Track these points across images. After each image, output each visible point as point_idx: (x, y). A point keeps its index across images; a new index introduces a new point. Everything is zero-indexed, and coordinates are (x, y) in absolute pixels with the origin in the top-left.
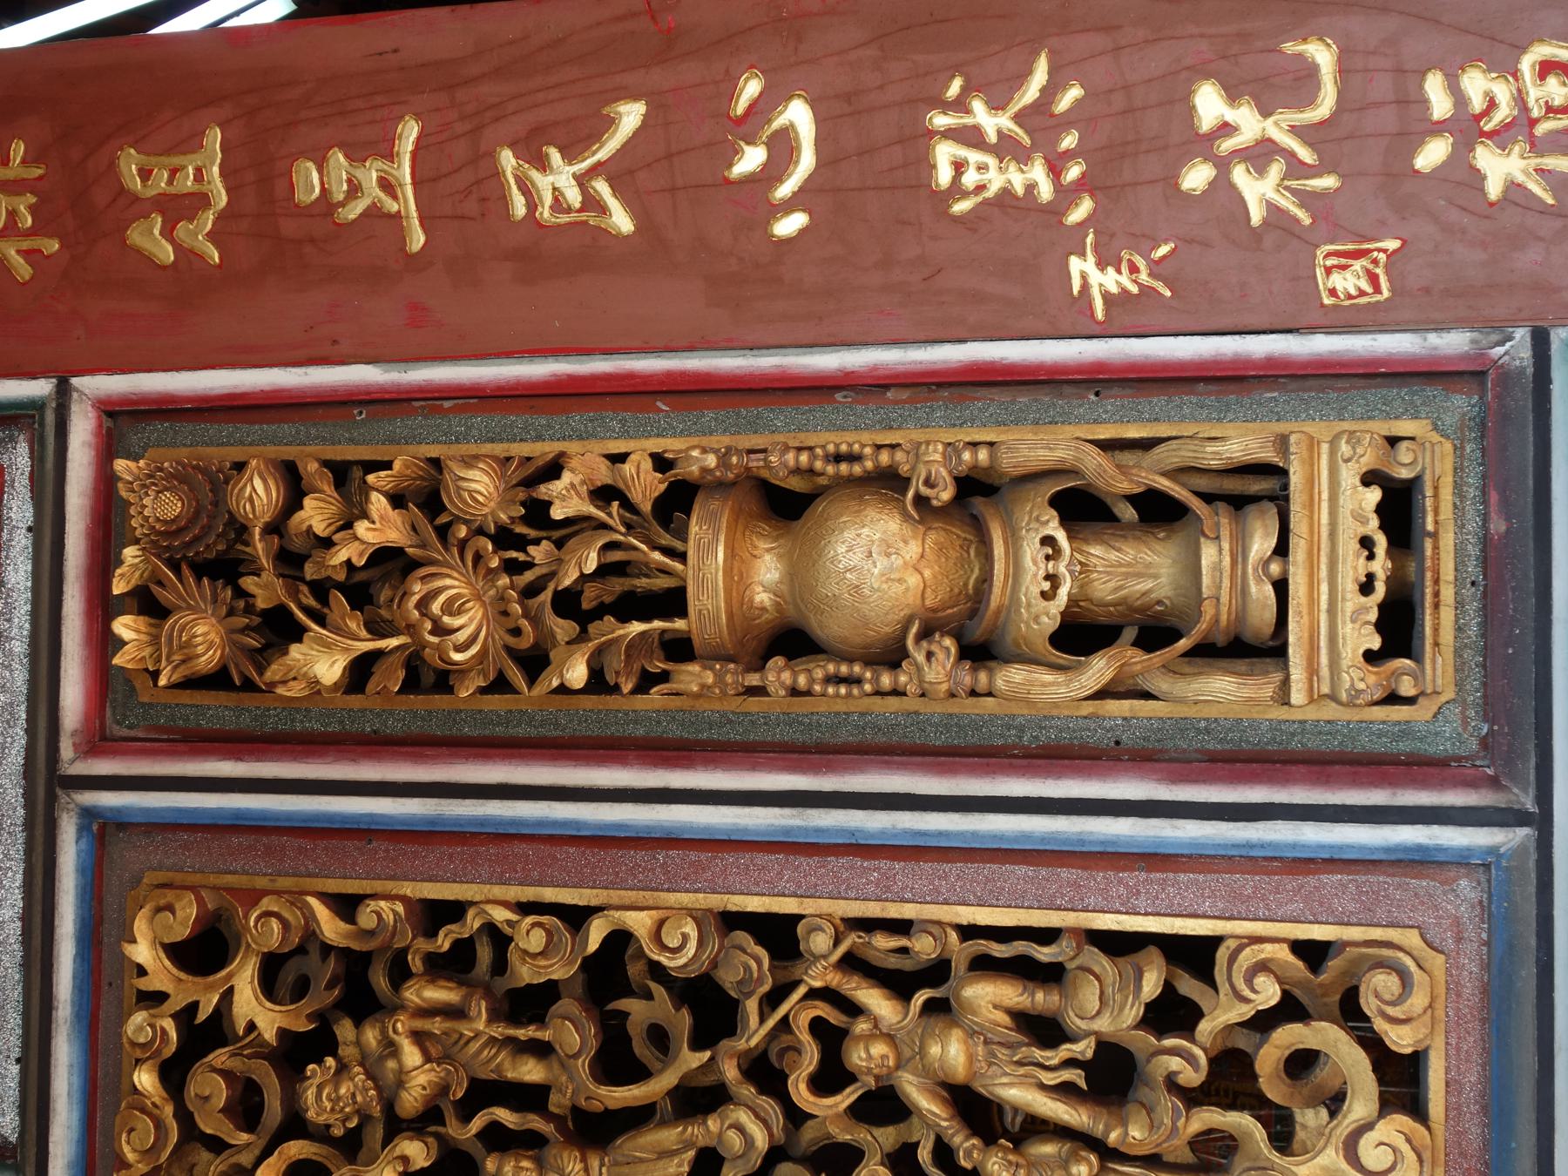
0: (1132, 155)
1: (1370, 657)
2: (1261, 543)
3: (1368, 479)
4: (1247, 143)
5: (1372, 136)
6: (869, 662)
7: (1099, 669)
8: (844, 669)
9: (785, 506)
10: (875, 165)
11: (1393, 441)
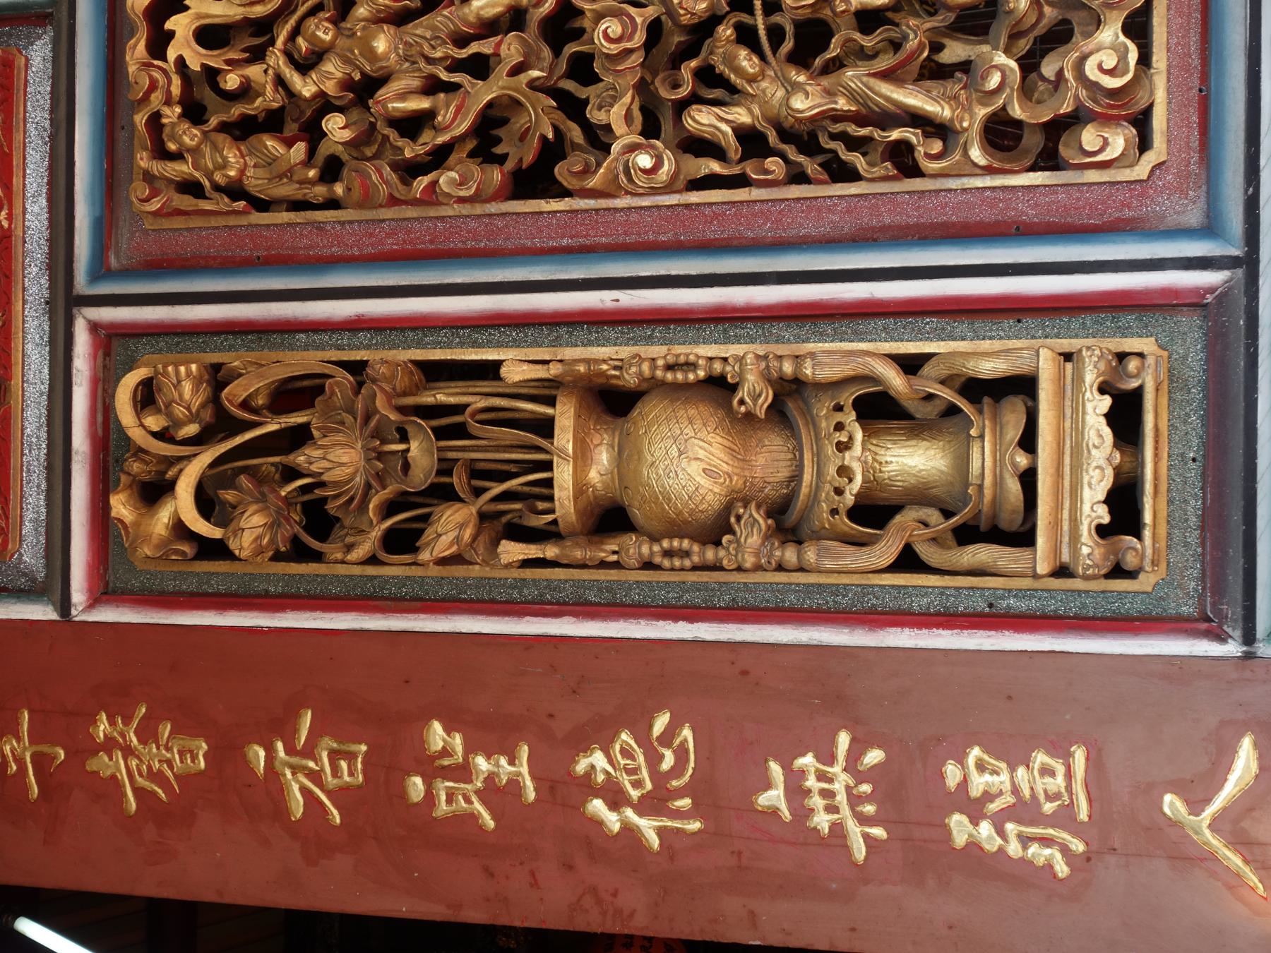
1: (1102, 531)
2: (1014, 431)
3: (1102, 390)
6: (693, 539)
7: (886, 550)
8: (680, 376)
9: (613, 402)
11: (1122, 357)
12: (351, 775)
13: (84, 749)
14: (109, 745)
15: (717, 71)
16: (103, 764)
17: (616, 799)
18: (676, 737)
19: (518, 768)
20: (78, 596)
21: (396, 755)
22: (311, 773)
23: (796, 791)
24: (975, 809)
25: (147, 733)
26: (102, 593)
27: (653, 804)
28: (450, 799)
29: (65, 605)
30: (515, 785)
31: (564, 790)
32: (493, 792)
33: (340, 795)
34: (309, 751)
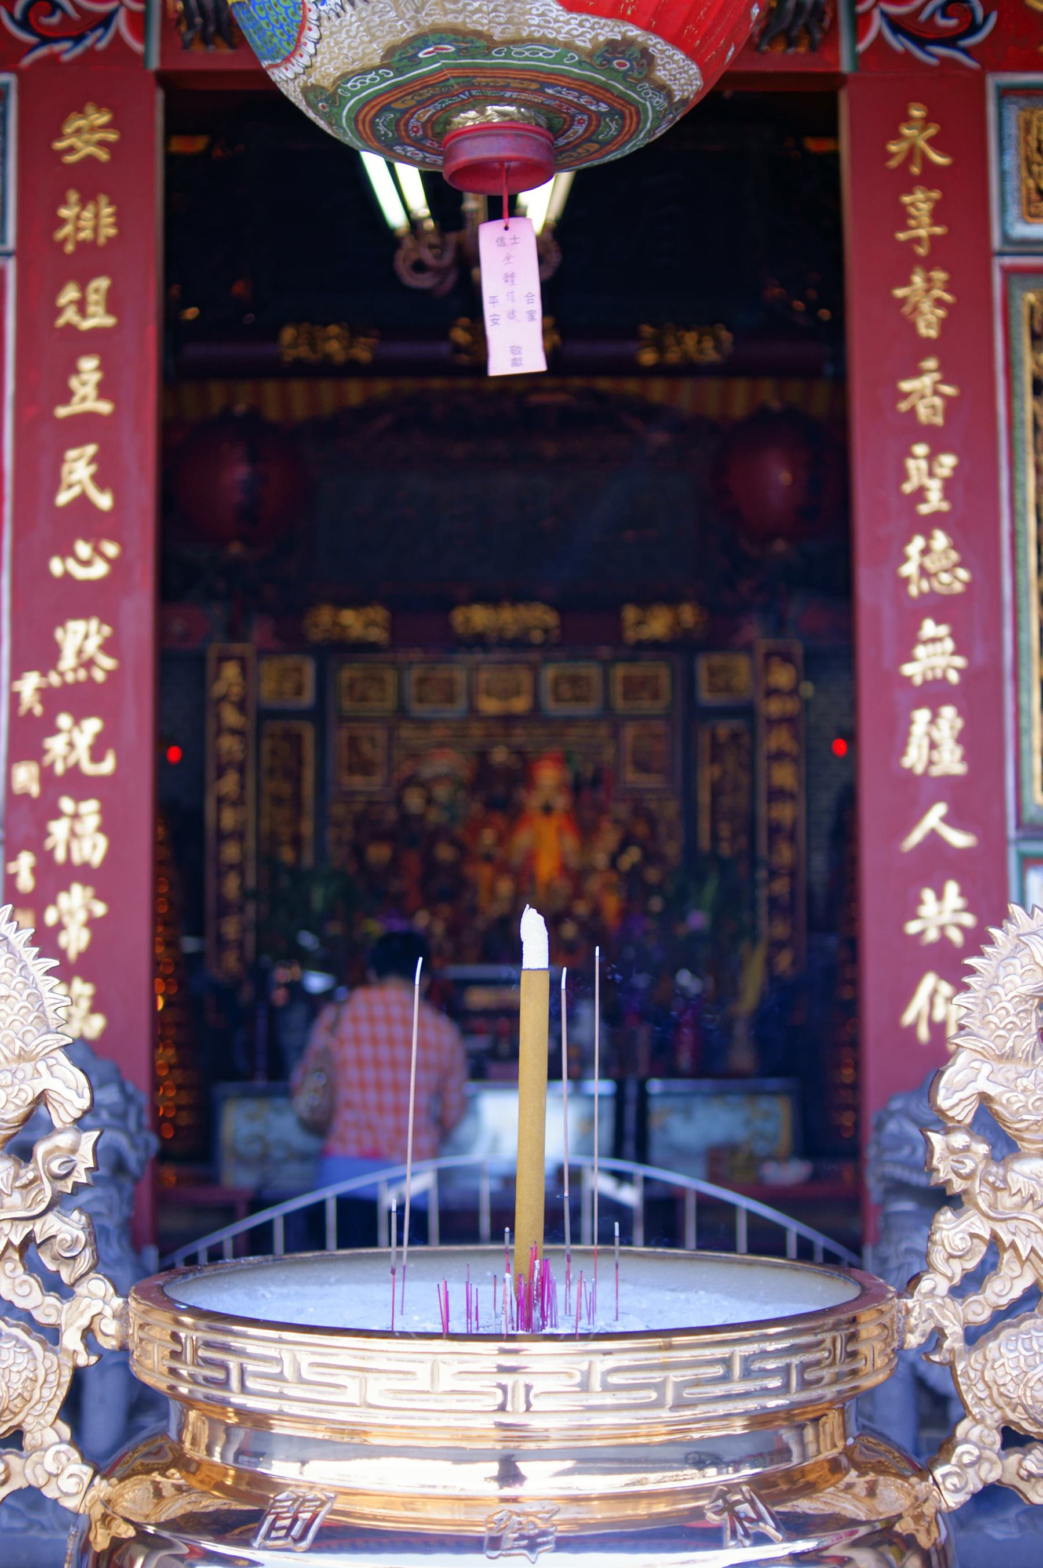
0: (77, 699)
4: (74, 741)
5: (76, 783)
10: (81, 600)
12: (923, 414)
13: (928, 264)
14: (929, 280)
15: (90, 109)
16: (918, 279)
17: (926, 551)
18: (955, 580)
19: (935, 501)
20: (1008, 261)
21: (938, 441)
22: (925, 392)
23: (934, 640)
24: (933, 721)
25: (939, 303)
26: (1008, 272)
27: (924, 572)
28: (916, 467)
29: (1002, 254)
30: (924, 500)
31: (926, 526)
32: (920, 494)
33: (913, 411)
34: (936, 393)
